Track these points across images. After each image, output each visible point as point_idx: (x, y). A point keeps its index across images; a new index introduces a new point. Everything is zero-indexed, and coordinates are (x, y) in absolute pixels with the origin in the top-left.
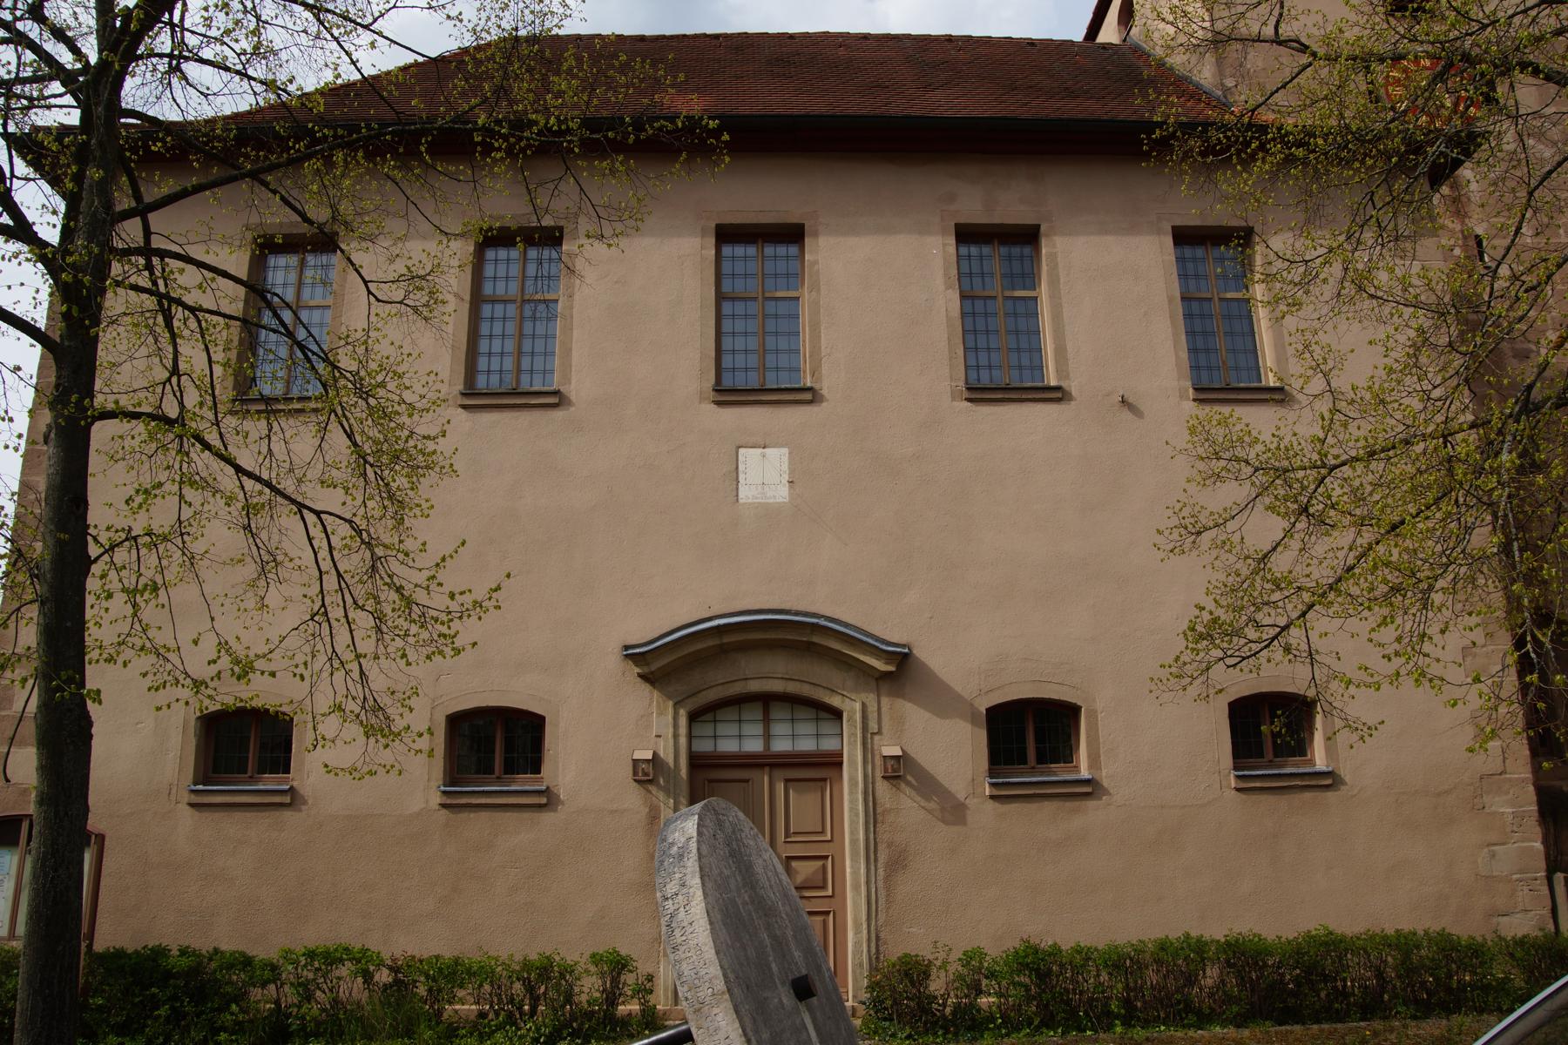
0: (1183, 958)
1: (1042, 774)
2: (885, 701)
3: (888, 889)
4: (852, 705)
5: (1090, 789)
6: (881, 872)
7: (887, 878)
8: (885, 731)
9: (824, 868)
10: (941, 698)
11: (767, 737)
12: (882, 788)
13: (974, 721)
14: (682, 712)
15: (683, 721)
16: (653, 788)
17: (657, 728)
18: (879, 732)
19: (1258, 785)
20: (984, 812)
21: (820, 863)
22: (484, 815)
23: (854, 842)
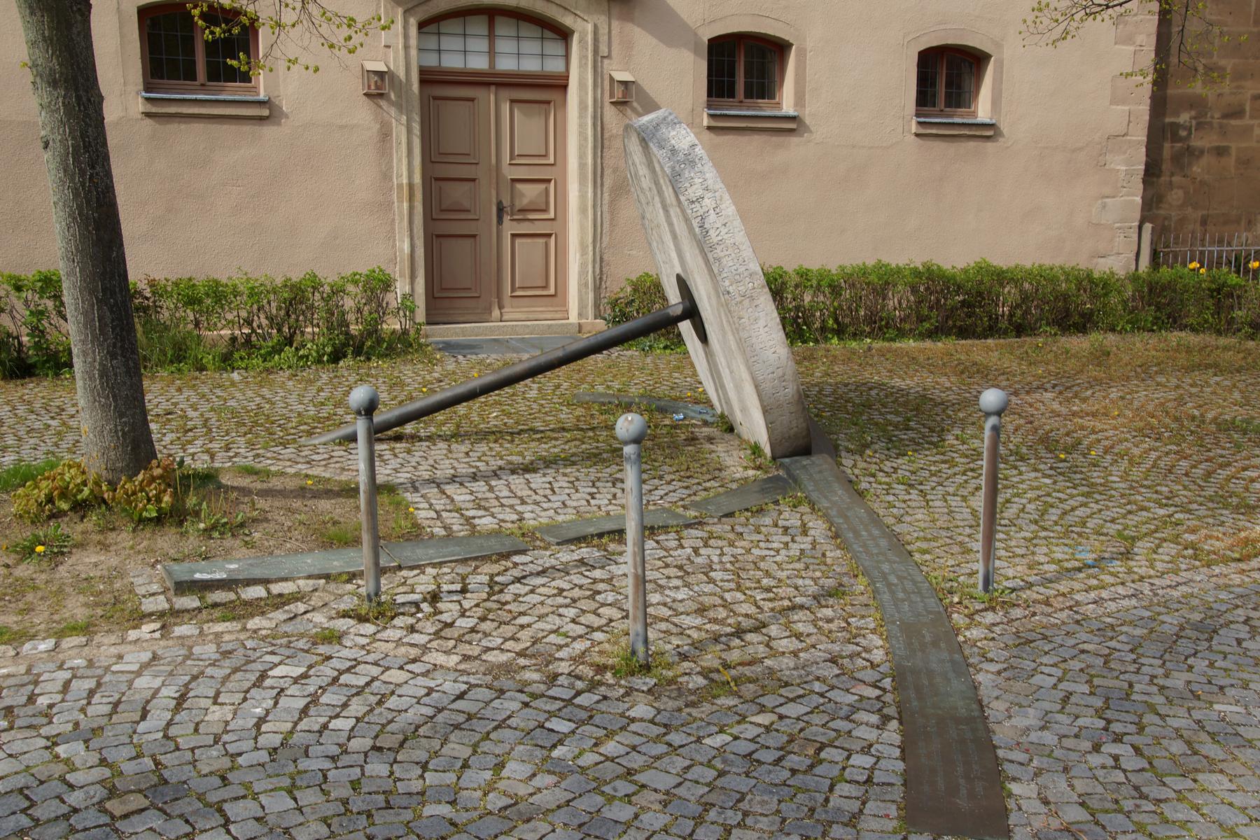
0: (880, 282)
1: (749, 108)
2: (615, 24)
3: (612, 213)
4: (583, 27)
5: (792, 126)
6: (606, 195)
7: (612, 202)
8: (614, 54)
9: (547, 191)
11: (492, 53)
12: (610, 113)
13: (696, 52)
14: (413, 22)
15: (413, 31)
16: (383, 103)
18: (609, 57)
19: (934, 131)
21: (542, 186)
22: (198, 127)
23: (582, 166)
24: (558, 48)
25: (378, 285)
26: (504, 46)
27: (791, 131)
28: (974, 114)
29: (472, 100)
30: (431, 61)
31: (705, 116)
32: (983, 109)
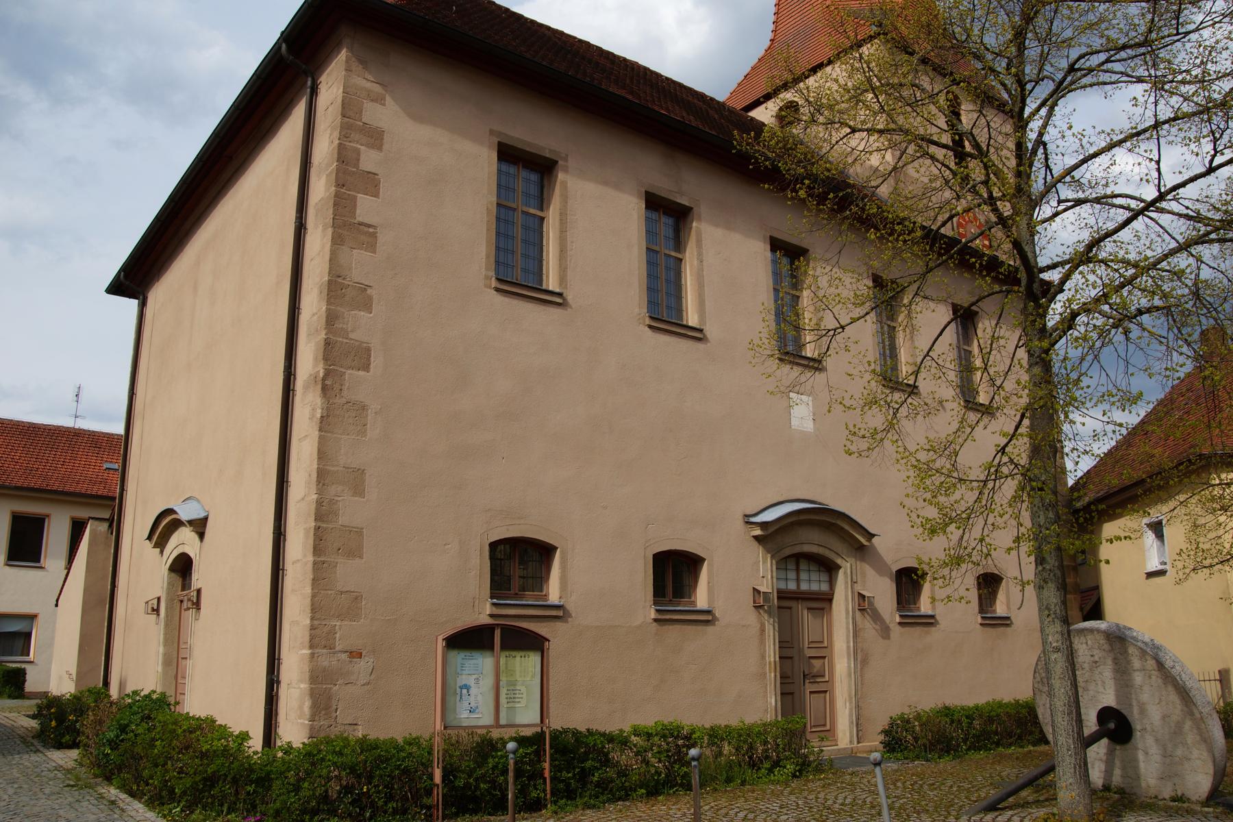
5: (707, 618)
10: (879, 565)
11: (798, 580)
12: (858, 614)
17: (762, 572)
20: (896, 631)
22: (678, 627)
24: (824, 577)
25: (245, 736)
26: (804, 576)
27: (556, 617)
28: (694, 603)
29: (790, 608)
30: (782, 586)
31: (488, 605)
32: (701, 599)
